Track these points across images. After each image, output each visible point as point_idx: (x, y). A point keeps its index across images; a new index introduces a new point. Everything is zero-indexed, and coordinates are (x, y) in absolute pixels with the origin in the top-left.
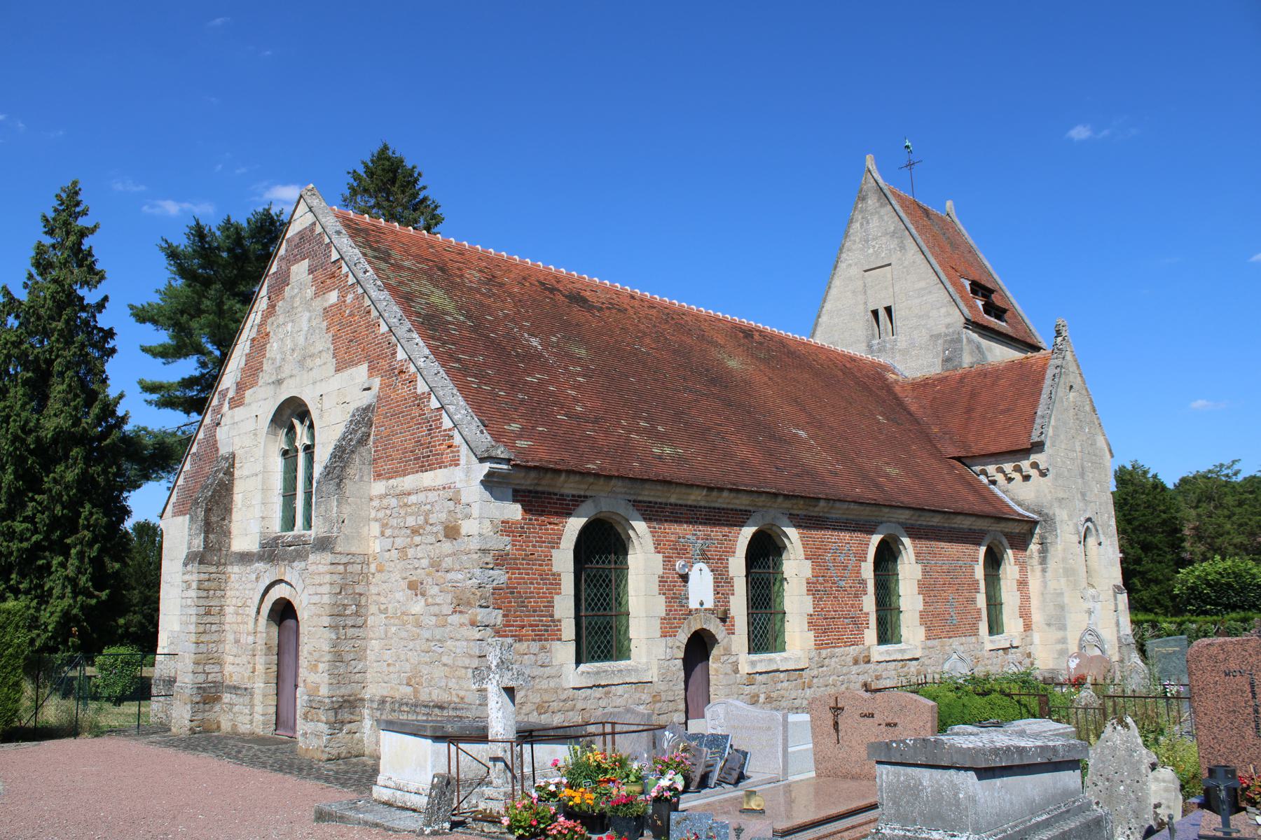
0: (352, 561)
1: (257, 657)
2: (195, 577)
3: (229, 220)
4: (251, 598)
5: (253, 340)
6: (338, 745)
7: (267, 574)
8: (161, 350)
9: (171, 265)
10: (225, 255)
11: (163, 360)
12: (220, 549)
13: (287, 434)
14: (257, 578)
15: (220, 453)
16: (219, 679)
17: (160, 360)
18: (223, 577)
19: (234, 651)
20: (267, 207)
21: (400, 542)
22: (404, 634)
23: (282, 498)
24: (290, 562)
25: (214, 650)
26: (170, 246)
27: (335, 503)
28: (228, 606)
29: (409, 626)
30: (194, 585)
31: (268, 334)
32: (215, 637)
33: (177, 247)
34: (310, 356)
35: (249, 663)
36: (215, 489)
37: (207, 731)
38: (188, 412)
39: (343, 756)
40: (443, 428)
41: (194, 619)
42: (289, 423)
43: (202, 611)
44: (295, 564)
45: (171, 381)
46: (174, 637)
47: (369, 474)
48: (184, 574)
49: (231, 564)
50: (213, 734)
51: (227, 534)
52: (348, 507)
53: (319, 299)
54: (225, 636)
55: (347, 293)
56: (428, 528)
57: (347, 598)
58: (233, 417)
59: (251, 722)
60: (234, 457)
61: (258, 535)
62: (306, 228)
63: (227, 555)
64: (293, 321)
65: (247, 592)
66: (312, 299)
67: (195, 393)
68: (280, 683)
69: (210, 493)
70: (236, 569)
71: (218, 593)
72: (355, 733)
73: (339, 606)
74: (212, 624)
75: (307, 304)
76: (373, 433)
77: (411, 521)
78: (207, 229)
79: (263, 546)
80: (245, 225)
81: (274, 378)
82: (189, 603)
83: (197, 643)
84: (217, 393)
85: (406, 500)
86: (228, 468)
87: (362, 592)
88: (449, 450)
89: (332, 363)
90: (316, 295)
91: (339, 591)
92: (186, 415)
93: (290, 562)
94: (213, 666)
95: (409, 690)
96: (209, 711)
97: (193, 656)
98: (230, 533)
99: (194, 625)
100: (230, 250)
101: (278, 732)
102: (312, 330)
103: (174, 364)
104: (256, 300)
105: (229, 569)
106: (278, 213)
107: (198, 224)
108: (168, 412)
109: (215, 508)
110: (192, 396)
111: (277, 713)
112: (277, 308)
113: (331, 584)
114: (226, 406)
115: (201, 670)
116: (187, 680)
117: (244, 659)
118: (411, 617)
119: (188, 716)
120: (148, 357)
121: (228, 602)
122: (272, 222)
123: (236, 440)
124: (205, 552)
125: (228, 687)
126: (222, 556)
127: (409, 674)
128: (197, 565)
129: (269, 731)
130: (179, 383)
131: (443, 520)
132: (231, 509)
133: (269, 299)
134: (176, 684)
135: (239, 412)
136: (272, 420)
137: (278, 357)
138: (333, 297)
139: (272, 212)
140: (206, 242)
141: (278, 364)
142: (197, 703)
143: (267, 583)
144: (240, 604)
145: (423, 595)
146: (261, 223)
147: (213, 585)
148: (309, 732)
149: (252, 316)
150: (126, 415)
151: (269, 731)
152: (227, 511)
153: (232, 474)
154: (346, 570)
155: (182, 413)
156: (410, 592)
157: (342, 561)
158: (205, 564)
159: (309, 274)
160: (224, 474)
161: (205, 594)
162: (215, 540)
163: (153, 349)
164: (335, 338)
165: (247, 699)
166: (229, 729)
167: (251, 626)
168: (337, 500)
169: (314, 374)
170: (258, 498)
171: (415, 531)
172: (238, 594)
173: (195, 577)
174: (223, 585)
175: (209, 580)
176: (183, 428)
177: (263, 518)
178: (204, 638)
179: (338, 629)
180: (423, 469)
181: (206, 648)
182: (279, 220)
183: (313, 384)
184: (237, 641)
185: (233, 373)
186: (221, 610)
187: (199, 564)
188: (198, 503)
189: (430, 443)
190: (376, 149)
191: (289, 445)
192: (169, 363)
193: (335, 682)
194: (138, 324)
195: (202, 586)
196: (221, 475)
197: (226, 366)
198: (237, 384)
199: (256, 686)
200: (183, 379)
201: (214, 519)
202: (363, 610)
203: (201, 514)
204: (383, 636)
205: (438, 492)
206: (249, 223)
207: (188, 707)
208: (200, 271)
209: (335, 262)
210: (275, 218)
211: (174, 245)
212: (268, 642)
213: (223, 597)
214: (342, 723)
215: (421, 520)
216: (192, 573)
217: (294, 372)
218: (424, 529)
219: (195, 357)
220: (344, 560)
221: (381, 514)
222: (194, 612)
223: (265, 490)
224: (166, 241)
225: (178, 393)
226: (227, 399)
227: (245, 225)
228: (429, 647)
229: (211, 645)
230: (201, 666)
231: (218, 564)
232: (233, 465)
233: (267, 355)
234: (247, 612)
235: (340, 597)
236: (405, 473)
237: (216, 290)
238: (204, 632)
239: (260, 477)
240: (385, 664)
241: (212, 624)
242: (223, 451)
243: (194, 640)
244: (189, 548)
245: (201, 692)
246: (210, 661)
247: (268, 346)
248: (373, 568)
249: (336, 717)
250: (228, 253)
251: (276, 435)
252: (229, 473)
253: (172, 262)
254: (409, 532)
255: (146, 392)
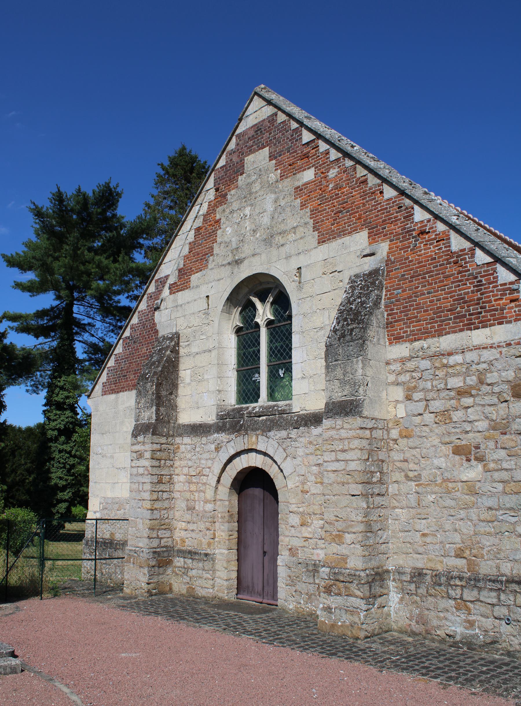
0: (375, 426)
1: (217, 524)
2: (148, 447)
3: (79, 190)
4: (209, 468)
5: (198, 229)
6: (372, 621)
7: (232, 443)
8: (29, 284)
9: (36, 223)
10: (75, 217)
11: (30, 294)
12: (169, 422)
13: (241, 313)
14: (218, 449)
15: (160, 334)
16: (170, 544)
17: (27, 294)
18: (172, 447)
19: (188, 517)
20: (107, 181)
21: (437, 405)
22: (449, 502)
23: (236, 373)
24: (263, 431)
25: (166, 516)
26: (37, 207)
27: (360, 365)
28: (177, 475)
29: (458, 494)
30: (148, 455)
31: (218, 221)
32: (166, 504)
33: (42, 208)
34: (280, 233)
35: (208, 529)
36: (164, 365)
37: (161, 593)
38: (37, 336)
39: (376, 632)
40: (499, 283)
41: (148, 487)
42: (244, 301)
43: (155, 479)
44: (271, 434)
45: (28, 313)
46: (107, 503)
47: (384, 338)
48: (132, 445)
49: (181, 435)
50: (168, 595)
51: (174, 407)
52: (371, 370)
53: (289, 179)
54: (174, 503)
55: (329, 168)
56: (485, 389)
57: (373, 465)
58: (175, 300)
59: (213, 586)
60: (178, 337)
61: (215, 407)
62: (264, 120)
63: (174, 427)
64: (252, 205)
65: (203, 462)
66: (277, 181)
67: (45, 322)
68: (242, 549)
69: (160, 369)
70: (187, 440)
71: (168, 463)
72: (384, 607)
73: (368, 473)
74: (163, 492)
75: (272, 187)
76: (383, 297)
77: (456, 382)
78: (65, 195)
79: (221, 418)
80: (91, 194)
81: (230, 259)
82: (141, 471)
83: (152, 510)
84: (154, 281)
85: (445, 361)
86: (174, 346)
87: (384, 458)
88: (513, 304)
89: (313, 237)
90: (282, 177)
91: (367, 457)
92: (35, 339)
93: (263, 431)
94: (165, 532)
95: (461, 563)
96: (163, 574)
97: (148, 522)
98: (176, 406)
99: (149, 493)
100: (79, 214)
101: (239, 596)
102: (279, 209)
103: (38, 296)
104: (200, 193)
105: (178, 440)
106: (115, 187)
107: (59, 190)
108: (24, 335)
109: (164, 383)
110: (42, 325)
111: (239, 578)
112: (229, 197)
113: (361, 449)
114: (166, 292)
115: (155, 536)
116: (141, 545)
117: (202, 526)
118: (460, 484)
119: (145, 579)
120: (18, 292)
121: (177, 471)
122: (111, 193)
123: (180, 321)
124: (157, 423)
125: (180, 551)
126: (171, 428)
127: (458, 546)
128: (150, 435)
129: (230, 596)
130: (34, 314)
131: (510, 379)
132: (177, 384)
133: (217, 190)
134: (127, 548)
135: (182, 296)
136: (228, 299)
137: (233, 239)
138: (309, 175)
139: (111, 186)
140: (64, 205)
141: (234, 246)
142: (153, 566)
143: (232, 452)
144: (194, 474)
145: (480, 459)
146: (103, 194)
147: (164, 455)
148: (333, 606)
149: (196, 208)
150: (5, 331)
151: (230, 596)
152: (175, 386)
153: (177, 352)
154: (371, 435)
155: (33, 337)
156: (457, 458)
157: (368, 426)
158: (157, 435)
159: (270, 160)
160: (171, 352)
161: (156, 463)
162: (164, 413)
163: (23, 284)
164: (314, 213)
165: (208, 565)
166: (184, 592)
167: (210, 494)
168: (362, 361)
169: (287, 248)
170: (214, 371)
171: (461, 393)
172: (190, 463)
173: (148, 447)
174: (172, 455)
175: (160, 450)
176: (38, 346)
177: (219, 391)
178: (157, 505)
179: (368, 498)
180: (470, 326)
181: (159, 514)
182: (115, 192)
183: (286, 258)
184: (190, 509)
185: (173, 262)
186: (170, 479)
187: (153, 435)
188: (147, 379)
189: (479, 299)
190: (178, 148)
191: (274, 316)
192: (34, 296)
193: (367, 554)
194: (9, 268)
195: (155, 456)
196: (168, 352)
197: (165, 256)
198: (180, 271)
199: (217, 551)
200: (38, 311)
201: (164, 393)
202: (385, 478)
203: (151, 388)
204: (414, 504)
205: (499, 349)
206: (94, 193)
207: (146, 570)
208: (57, 228)
209: (308, 144)
210: (113, 190)
211: (40, 206)
212: (230, 510)
213: (172, 466)
214: (375, 597)
215: (472, 380)
216: (144, 443)
217: (257, 251)
218: (479, 390)
219: (53, 291)
220: (370, 425)
221: (405, 378)
222: (149, 481)
223: (221, 364)
224: (34, 204)
225: (33, 322)
226: (167, 286)
227: (91, 194)
228: (496, 515)
229: (163, 512)
230: (155, 532)
231: (168, 436)
232: (178, 344)
233: (219, 240)
234: (205, 481)
235: (368, 463)
236: (440, 333)
237: (74, 237)
238: (157, 500)
239: (214, 353)
240: (418, 534)
241: (163, 492)
242: (164, 331)
243: (149, 507)
244: (137, 420)
245: (156, 556)
246: (163, 527)
247: (219, 232)
248: (394, 433)
249: (370, 591)
250: (77, 215)
251: (229, 313)
252: (175, 351)
253: (37, 221)
254: (453, 393)
255: (9, 320)
